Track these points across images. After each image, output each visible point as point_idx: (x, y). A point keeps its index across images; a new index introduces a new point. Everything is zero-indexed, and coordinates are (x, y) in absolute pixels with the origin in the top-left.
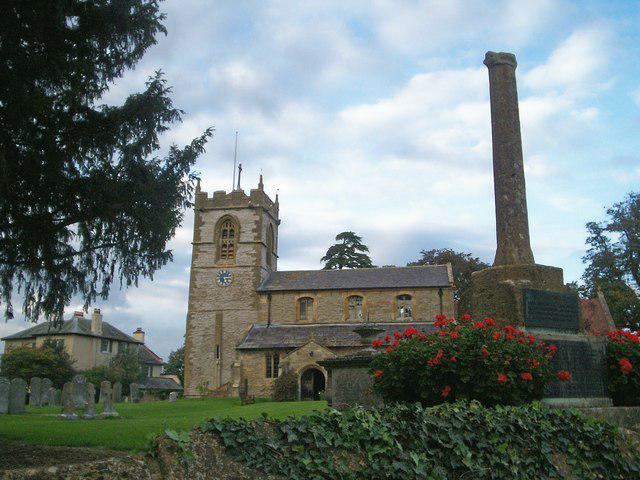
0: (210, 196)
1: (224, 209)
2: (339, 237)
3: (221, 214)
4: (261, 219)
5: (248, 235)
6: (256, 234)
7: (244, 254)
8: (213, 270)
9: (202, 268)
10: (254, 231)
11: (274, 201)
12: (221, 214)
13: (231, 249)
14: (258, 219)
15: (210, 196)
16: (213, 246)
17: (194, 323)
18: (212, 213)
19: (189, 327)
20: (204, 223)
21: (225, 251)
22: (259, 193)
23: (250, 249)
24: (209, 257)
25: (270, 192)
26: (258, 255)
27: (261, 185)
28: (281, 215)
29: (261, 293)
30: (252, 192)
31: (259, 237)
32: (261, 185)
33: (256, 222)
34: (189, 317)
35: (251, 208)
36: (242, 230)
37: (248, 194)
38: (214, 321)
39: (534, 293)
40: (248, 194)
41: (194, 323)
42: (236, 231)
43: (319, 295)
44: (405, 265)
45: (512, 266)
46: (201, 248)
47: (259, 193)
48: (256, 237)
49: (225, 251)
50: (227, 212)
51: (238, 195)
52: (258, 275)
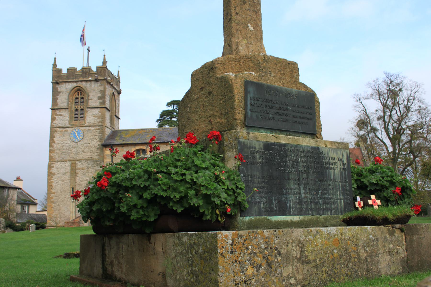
0: (65, 71)
1: (76, 82)
2: (169, 104)
3: (75, 85)
4: (105, 88)
5: (94, 101)
6: (101, 101)
7: (91, 116)
8: (67, 129)
9: (59, 127)
10: (99, 98)
11: (116, 74)
12: (75, 85)
13: (82, 116)
14: (103, 89)
15: (65, 71)
16: (67, 111)
17: (53, 170)
18: (64, 85)
19: (50, 174)
20: (60, 92)
21: (78, 115)
22: (103, 69)
23: (96, 112)
24: (64, 118)
25: (112, 68)
26: (103, 118)
27: (105, 62)
28: (122, 86)
29: (105, 146)
30: (98, 68)
31: (104, 103)
32: (105, 62)
33: (101, 91)
34: (50, 167)
35: (96, 80)
36: (89, 98)
37: (94, 69)
38: (69, 168)
39: (259, 86)
40: (94, 69)
41: (53, 170)
42: (86, 98)
43: (148, 142)
44: (188, 86)
45: (268, 104)
46: (58, 112)
47: (103, 69)
48: (101, 103)
49: (78, 115)
50: (79, 84)
51: (86, 71)
52: (102, 132)
